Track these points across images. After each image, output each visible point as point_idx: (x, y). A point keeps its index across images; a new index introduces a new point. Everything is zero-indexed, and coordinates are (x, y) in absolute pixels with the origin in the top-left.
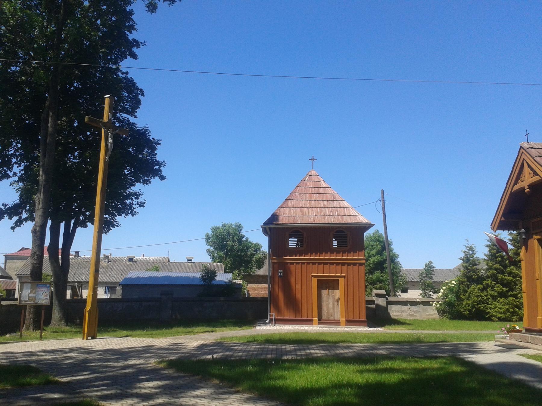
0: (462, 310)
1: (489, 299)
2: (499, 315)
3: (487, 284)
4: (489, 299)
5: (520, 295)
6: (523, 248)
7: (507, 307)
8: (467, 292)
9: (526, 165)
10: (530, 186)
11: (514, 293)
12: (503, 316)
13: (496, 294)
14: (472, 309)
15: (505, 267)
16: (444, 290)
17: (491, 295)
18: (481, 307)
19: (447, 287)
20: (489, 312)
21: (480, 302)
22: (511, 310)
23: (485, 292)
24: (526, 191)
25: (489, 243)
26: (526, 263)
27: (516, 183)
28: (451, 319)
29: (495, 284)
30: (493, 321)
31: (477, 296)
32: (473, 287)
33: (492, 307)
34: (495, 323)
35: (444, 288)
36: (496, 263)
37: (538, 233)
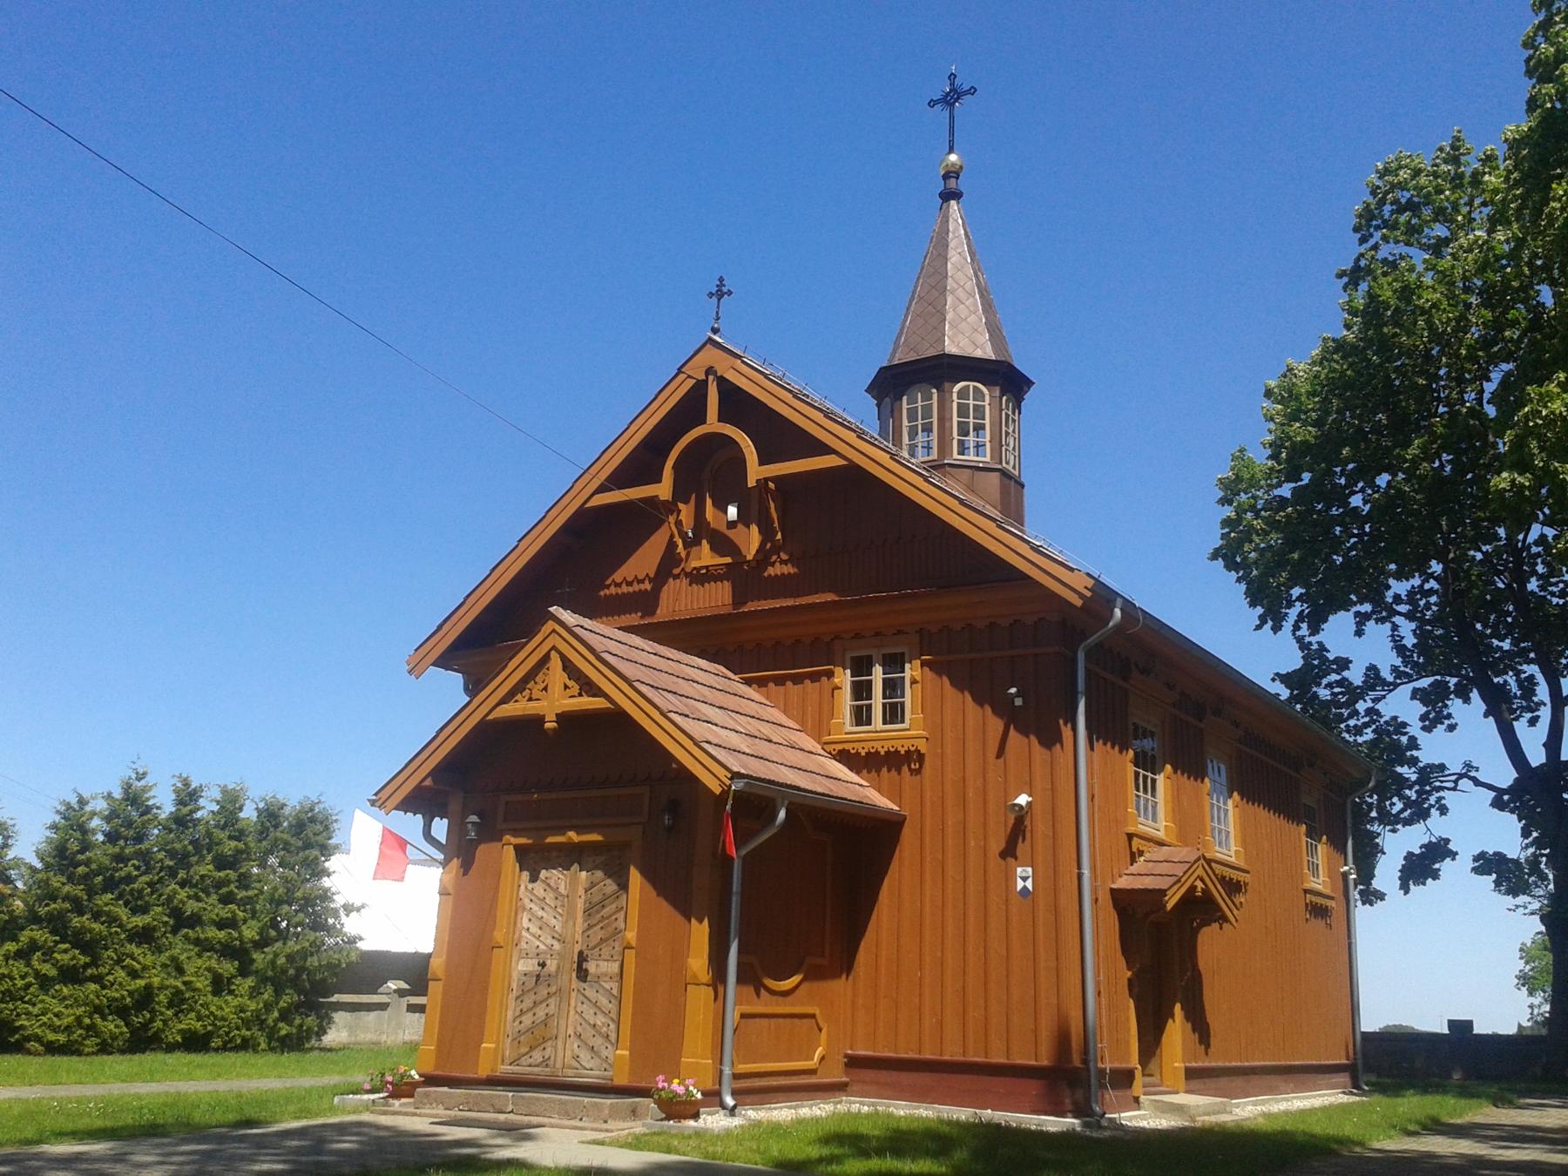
2: (51, 1037)
3: (33, 942)
4: (28, 986)
5: (111, 978)
7: (80, 1011)
9: (556, 661)
10: (562, 718)
11: (103, 970)
12: (62, 1038)
13: (53, 972)
15: (91, 892)
17: (37, 974)
20: (22, 1027)
24: (547, 725)
27: (508, 697)
29: (57, 943)
30: (29, 1053)
33: (35, 1010)
36: (70, 879)
37: (523, 830)
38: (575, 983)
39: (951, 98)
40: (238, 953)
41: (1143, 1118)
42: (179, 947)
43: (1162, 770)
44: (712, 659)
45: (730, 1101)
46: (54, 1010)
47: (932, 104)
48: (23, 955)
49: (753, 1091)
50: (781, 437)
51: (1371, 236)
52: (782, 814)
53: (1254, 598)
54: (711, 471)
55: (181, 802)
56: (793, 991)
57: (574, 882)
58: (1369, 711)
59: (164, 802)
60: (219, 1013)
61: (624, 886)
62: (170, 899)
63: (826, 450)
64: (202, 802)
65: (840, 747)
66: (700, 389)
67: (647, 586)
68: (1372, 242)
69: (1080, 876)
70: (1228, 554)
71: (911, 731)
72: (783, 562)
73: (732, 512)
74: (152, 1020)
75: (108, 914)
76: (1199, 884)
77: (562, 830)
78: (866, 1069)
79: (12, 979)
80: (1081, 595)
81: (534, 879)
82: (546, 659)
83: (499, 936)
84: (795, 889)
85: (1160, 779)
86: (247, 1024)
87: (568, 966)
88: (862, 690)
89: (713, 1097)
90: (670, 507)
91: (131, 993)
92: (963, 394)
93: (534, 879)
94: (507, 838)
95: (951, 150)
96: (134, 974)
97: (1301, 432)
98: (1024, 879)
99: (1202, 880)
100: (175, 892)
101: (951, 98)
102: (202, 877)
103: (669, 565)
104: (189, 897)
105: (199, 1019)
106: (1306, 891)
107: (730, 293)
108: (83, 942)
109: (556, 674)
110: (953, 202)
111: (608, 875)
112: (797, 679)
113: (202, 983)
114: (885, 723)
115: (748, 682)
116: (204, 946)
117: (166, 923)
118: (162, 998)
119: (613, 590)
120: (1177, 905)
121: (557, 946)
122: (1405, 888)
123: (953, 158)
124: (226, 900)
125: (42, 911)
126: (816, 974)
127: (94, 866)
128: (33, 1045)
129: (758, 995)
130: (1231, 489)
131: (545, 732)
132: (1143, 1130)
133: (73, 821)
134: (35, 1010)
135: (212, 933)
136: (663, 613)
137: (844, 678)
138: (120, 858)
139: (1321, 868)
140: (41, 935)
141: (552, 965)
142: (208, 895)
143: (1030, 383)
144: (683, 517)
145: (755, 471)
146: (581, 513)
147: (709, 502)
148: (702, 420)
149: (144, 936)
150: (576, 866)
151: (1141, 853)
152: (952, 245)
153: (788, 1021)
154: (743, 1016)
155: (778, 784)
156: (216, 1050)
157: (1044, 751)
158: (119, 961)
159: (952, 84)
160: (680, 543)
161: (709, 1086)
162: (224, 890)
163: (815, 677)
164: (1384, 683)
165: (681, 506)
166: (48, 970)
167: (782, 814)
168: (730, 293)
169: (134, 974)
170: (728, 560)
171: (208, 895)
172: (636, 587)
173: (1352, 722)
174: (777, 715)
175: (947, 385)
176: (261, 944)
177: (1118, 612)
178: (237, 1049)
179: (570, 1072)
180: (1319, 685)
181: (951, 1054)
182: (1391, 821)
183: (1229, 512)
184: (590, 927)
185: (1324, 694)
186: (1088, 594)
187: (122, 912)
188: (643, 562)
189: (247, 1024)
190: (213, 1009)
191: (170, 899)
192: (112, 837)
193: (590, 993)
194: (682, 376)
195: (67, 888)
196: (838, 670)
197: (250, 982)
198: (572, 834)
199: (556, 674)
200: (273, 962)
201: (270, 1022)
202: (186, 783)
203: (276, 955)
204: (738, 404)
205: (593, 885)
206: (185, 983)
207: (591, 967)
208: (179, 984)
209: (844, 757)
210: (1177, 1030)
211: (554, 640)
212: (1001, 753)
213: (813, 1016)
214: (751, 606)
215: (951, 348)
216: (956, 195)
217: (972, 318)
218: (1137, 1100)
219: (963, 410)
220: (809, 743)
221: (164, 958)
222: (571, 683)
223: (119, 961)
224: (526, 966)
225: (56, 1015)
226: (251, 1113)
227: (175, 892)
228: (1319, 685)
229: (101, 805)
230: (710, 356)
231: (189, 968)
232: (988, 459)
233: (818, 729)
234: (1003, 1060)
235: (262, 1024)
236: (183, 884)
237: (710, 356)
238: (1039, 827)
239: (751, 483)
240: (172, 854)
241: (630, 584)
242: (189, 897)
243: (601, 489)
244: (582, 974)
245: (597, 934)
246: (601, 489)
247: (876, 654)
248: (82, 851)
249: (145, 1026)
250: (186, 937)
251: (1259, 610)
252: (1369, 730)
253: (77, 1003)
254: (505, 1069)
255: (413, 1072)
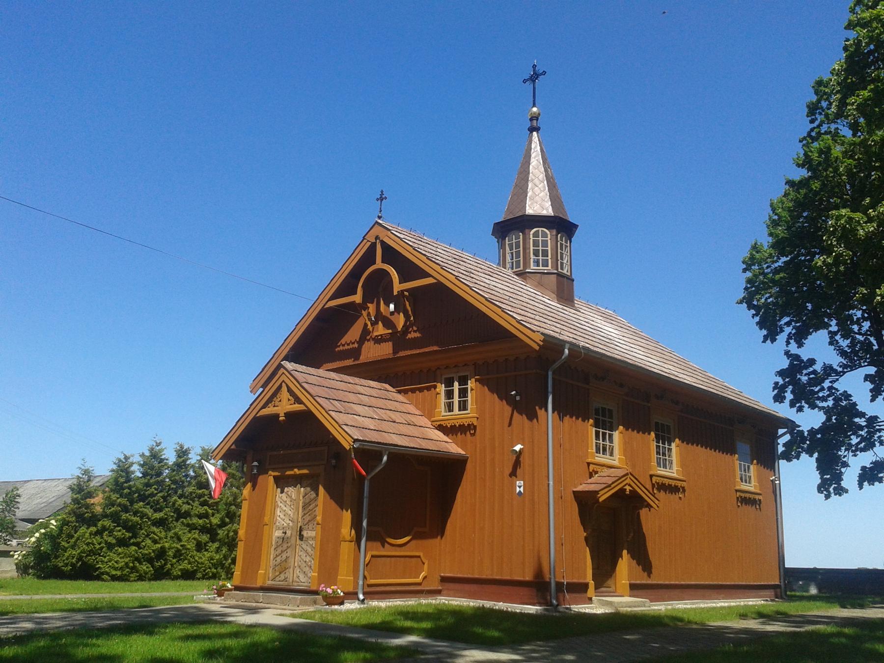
0: (60, 565)
1: (103, 548)
2: (114, 572)
4: (103, 548)
6: (249, 485)
7: (127, 560)
8: (72, 537)
9: (284, 388)
10: (287, 415)
11: (138, 540)
12: (119, 573)
13: (114, 541)
14: (77, 562)
15: (132, 502)
16: (41, 534)
17: (106, 542)
18: (91, 559)
19: (48, 530)
21: (92, 552)
22: (131, 565)
23: (98, 538)
25: (115, 467)
26: (249, 505)
27: (264, 407)
28: (39, 577)
29: (115, 527)
30: (103, 580)
31: (88, 544)
32: (83, 530)
33: (106, 560)
34: (106, 583)
35: (43, 531)
36: (121, 496)
38: (298, 541)
39: (534, 77)
40: (211, 531)
41: (592, 608)
42: (178, 528)
43: (617, 429)
44: (379, 380)
45: (361, 597)
46: (116, 559)
47: (525, 81)
48: (99, 533)
49: (372, 593)
50: (409, 270)
51: (817, 119)
52: (385, 458)
53: (761, 325)
54: (378, 287)
55: (179, 457)
56: (405, 545)
57: (299, 493)
58: (830, 388)
59: (171, 457)
60: (200, 561)
61: (317, 495)
62: (174, 504)
63: (428, 275)
64: (190, 456)
65: (438, 423)
66: (373, 246)
67: (356, 345)
68: (817, 123)
69: (549, 485)
70: (748, 301)
71: (470, 414)
72: (415, 331)
73: (392, 306)
74: (165, 564)
75: (142, 512)
76: (628, 488)
77: (292, 469)
78: (451, 583)
79: (93, 544)
80: (538, 345)
81: (282, 492)
82: (280, 387)
83: (266, 519)
84: (404, 496)
85: (616, 435)
86: (215, 566)
87: (294, 533)
88: (449, 394)
89: (351, 595)
90: (363, 306)
91: (154, 551)
92: (536, 235)
93: (282, 492)
94: (270, 472)
95: (534, 105)
96: (155, 542)
97: (780, 231)
98: (520, 487)
99: (630, 485)
100: (176, 501)
101: (534, 77)
102: (191, 493)
103: (365, 332)
104: (183, 503)
105: (190, 563)
106: (737, 491)
107: (386, 198)
108: (132, 529)
109: (284, 394)
110: (535, 133)
111: (312, 489)
112: (421, 390)
113: (191, 546)
114: (459, 410)
115: (399, 392)
116: (192, 527)
117: (172, 516)
118: (171, 553)
119: (341, 348)
120: (605, 500)
121: (291, 524)
122: (861, 486)
123: (535, 109)
124: (203, 504)
125: (108, 511)
126: (418, 536)
127: (133, 489)
128: (105, 577)
129: (383, 546)
130: (749, 264)
131: (280, 421)
132: (585, 614)
133: (123, 468)
134: (106, 560)
135: (195, 520)
136: (363, 359)
137: (442, 388)
138: (148, 485)
139: (750, 479)
140: (107, 523)
141: (289, 533)
142: (194, 501)
143: (576, 226)
144: (371, 310)
145: (397, 287)
146: (323, 311)
147: (382, 302)
148: (374, 263)
149: (161, 523)
150: (299, 486)
151: (596, 473)
152: (533, 156)
153: (402, 559)
154: (372, 556)
155: (383, 444)
156: (199, 579)
157: (530, 422)
158: (148, 536)
159: (534, 70)
160: (369, 323)
161: (351, 589)
162: (202, 499)
163: (428, 389)
164: (835, 371)
165: (369, 305)
166: (111, 540)
167: (385, 458)
168: (386, 198)
169: (155, 542)
170: (390, 331)
171: (194, 501)
172: (351, 346)
173: (821, 394)
174: (412, 409)
175: (527, 231)
176: (223, 524)
177: (567, 351)
178: (209, 578)
179: (295, 584)
180: (801, 374)
181: (486, 575)
182: (856, 450)
183: (749, 274)
184: (305, 514)
185: (804, 379)
186: (541, 343)
187: (149, 511)
188: (354, 334)
189: (215, 566)
190: (197, 558)
191: (174, 504)
192: (145, 475)
193: (304, 546)
194: (365, 241)
195: (119, 501)
196: (439, 385)
197: (216, 545)
198: (296, 470)
199: (284, 394)
200: (228, 534)
201: (227, 565)
202: (182, 447)
203: (229, 531)
204: (392, 255)
205: (306, 494)
206: (181, 546)
207: (305, 533)
208: (179, 546)
209: (440, 428)
210: (625, 565)
211: (283, 378)
212: (510, 424)
213: (419, 557)
214: (402, 354)
215: (529, 211)
216: (537, 129)
217: (542, 194)
218: (590, 599)
219: (536, 244)
220: (424, 421)
221: (171, 534)
222: (291, 398)
223: (148, 536)
224: (278, 533)
225: (116, 562)
226: (148, 603)
227: (176, 501)
228: (801, 374)
229: (137, 459)
230: (377, 230)
231: (184, 539)
232: (550, 268)
233: (429, 413)
234: (508, 578)
235: (223, 566)
236: (180, 497)
237: (377, 230)
238: (525, 460)
239: (395, 293)
240: (174, 482)
241: (348, 345)
242: (183, 503)
243: (333, 298)
244: (301, 537)
245: (307, 518)
246: (333, 298)
247: (455, 376)
248: (126, 482)
249: (162, 567)
250: (182, 522)
251: (764, 332)
252: (831, 399)
253: (126, 556)
254: (269, 583)
255: (339, 591)
